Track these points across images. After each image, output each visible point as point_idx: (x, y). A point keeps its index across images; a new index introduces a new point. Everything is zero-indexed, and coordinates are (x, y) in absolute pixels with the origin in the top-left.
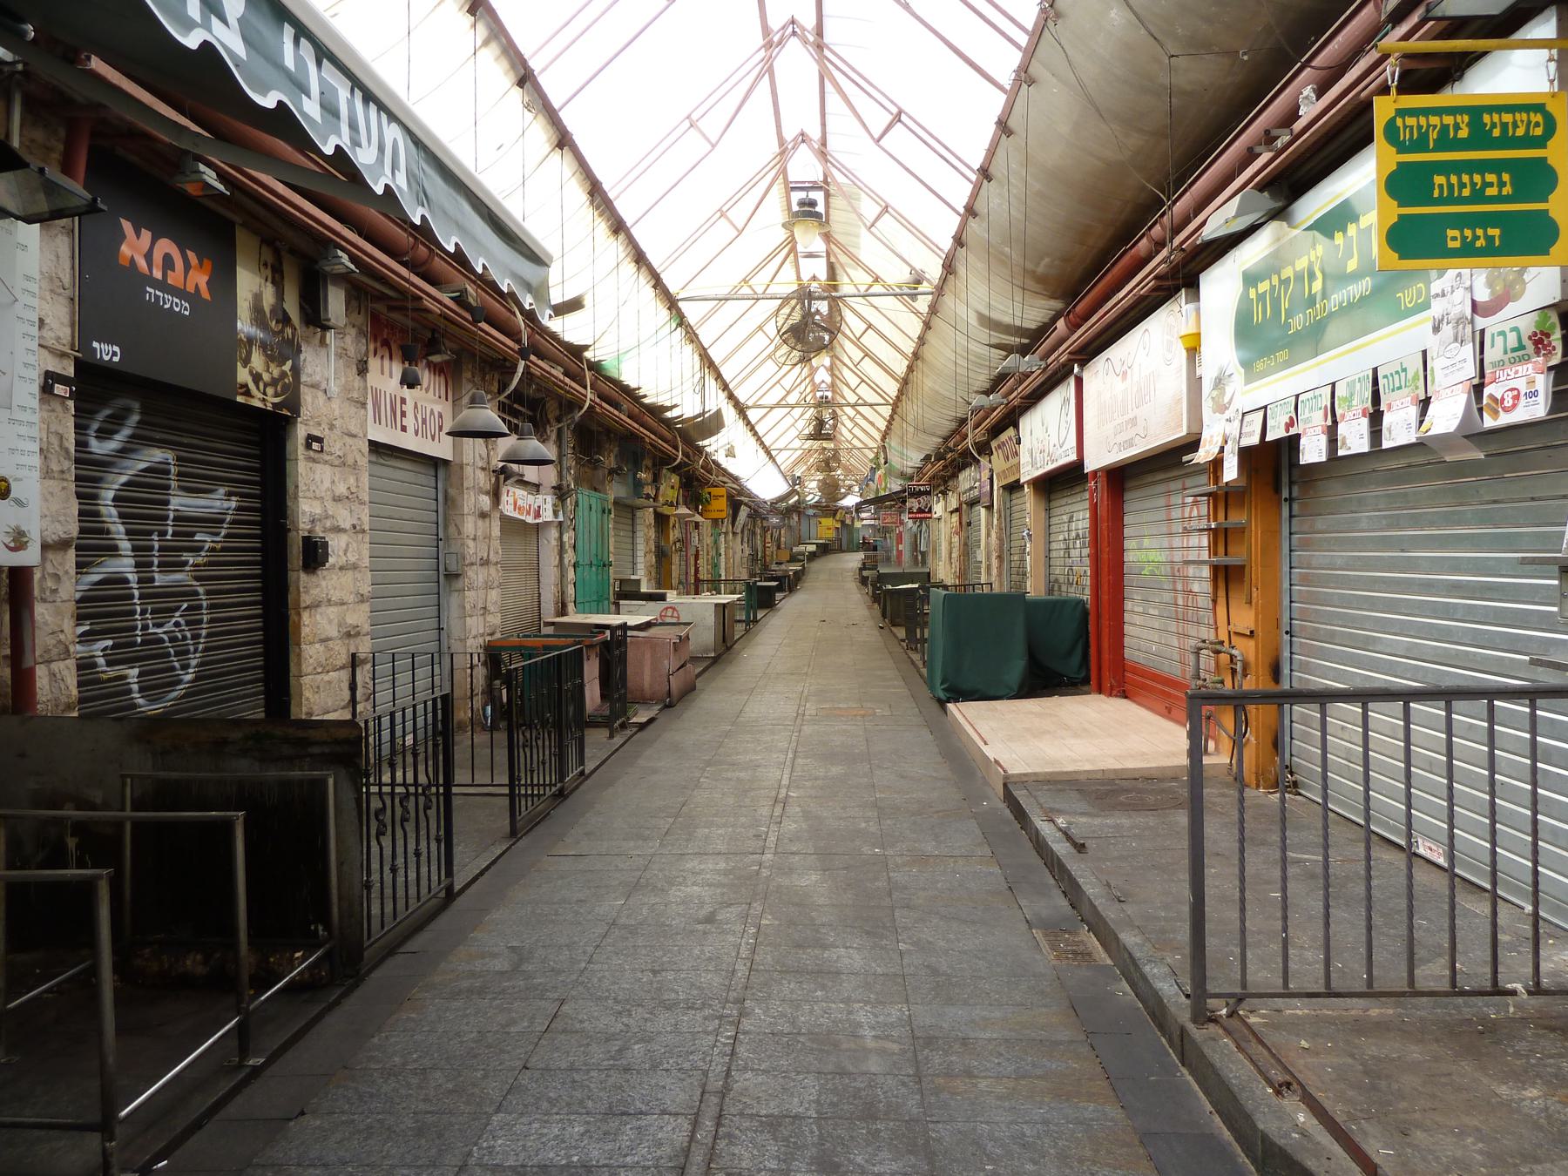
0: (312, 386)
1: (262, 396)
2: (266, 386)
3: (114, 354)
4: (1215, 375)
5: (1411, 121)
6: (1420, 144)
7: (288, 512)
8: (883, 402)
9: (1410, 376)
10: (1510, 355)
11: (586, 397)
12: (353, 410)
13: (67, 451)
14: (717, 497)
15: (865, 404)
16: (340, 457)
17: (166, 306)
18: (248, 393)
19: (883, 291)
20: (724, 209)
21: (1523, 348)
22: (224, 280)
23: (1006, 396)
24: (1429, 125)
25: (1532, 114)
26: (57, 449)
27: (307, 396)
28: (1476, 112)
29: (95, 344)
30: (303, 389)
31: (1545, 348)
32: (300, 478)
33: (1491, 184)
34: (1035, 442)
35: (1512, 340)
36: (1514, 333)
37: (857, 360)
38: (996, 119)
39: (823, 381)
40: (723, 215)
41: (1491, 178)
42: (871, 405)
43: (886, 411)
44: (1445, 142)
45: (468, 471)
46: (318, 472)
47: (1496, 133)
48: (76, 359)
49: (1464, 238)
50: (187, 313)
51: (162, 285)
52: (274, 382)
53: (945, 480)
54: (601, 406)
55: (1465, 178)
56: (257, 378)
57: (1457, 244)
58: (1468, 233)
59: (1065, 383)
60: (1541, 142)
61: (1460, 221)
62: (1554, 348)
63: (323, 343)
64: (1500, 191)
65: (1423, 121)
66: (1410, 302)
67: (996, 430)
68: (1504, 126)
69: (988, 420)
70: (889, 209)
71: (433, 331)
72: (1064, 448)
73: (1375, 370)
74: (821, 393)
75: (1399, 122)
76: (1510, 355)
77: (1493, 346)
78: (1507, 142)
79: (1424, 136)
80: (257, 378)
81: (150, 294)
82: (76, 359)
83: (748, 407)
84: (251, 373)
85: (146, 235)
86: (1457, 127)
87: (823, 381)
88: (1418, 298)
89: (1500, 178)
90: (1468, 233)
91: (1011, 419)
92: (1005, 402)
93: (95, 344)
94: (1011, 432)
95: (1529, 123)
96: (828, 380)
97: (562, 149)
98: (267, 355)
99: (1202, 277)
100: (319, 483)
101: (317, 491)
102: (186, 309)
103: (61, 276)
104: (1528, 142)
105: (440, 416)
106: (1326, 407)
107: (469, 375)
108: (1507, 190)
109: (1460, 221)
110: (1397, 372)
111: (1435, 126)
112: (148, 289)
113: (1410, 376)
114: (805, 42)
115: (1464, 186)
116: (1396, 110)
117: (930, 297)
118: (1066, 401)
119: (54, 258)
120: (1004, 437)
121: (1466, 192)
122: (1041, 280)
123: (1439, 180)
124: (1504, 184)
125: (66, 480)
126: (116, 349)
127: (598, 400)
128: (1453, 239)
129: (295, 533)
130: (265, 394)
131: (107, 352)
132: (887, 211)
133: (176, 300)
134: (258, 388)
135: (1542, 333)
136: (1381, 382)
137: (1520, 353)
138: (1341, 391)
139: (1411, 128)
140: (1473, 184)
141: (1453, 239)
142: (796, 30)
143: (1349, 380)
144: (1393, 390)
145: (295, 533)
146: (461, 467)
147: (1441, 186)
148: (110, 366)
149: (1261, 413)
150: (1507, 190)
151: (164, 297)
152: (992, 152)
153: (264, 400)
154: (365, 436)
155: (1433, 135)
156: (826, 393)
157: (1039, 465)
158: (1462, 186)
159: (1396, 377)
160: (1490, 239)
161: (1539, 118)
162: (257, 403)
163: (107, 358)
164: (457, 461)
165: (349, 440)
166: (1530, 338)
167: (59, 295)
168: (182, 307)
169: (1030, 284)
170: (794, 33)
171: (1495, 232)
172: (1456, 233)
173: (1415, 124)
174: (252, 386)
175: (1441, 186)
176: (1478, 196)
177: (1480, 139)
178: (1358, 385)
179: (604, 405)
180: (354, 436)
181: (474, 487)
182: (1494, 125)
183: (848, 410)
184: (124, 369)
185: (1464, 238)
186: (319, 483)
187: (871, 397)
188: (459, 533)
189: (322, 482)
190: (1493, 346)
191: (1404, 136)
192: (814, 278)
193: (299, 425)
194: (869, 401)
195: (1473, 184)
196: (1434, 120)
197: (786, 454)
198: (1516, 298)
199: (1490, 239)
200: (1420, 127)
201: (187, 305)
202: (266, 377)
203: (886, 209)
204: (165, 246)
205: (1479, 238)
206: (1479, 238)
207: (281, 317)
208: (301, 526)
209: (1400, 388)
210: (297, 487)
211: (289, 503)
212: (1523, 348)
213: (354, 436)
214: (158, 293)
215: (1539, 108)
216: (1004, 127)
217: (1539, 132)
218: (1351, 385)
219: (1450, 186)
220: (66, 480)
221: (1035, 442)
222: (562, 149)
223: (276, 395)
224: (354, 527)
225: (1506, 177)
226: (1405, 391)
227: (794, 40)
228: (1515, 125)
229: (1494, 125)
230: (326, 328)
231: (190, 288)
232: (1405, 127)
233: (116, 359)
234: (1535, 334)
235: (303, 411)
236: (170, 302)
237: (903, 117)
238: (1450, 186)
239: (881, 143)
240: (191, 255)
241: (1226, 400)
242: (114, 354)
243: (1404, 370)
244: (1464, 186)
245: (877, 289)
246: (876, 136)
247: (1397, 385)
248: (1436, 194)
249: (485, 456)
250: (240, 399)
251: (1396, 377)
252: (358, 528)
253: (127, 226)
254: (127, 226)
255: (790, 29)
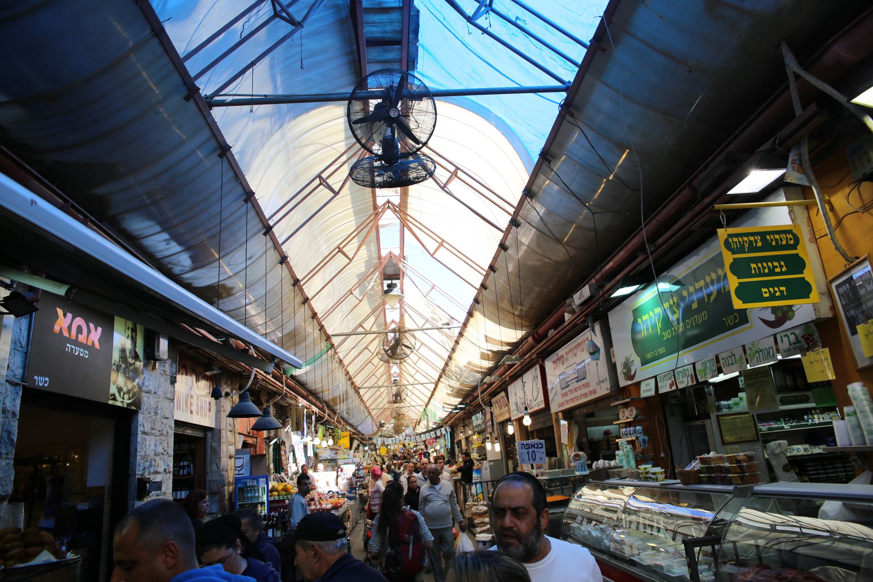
0: (147, 392)
1: (122, 400)
2: (124, 394)
3: (46, 382)
4: (624, 361)
5: (735, 240)
6: (741, 250)
7: (131, 465)
8: (429, 382)
9: (737, 358)
10: (793, 346)
11: (283, 388)
12: (167, 404)
13: (12, 440)
14: (344, 437)
15: (420, 384)
16: (159, 431)
17: (76, 354)
18: (115, 399)
19: (430, 326)
20: (341, 246)
21: (800, 342)
22: (107, 338)
23: (500, 376)
24: (743, 241)
25: (787, 235)
26: (6, 440)
27: (145, 397)
28: (763, 234)
29: (36, 377)
30: (143, 394)
31: (811, 341)
32: (138, 445)
33: (777, 267)
34: (518, 399)
35: (792, 337)
36: (786, 338)
37: (415, 361)
38: (499, 244)
39: (395, 372)
40: (340, 251)
41: (776, 264)
42: (422, 384)
43: (433, 386)
44: (752, 249)
45: (223, 433)
46: (148, 440)
47: (774, 243)
48: (24, 387)
49: (770, 292)
50: (87, 357)
51: (76, 343)
52: (129, 392)
53: (464, 420)
54: (289, 393)
55: (765, 265)
56: (120, 390)
57: (767, 295)
58: (771, 289)
59: (534, 368)
60: (794, 247)
61: (767, 284)
62: (817, 342)
63: (154, 368)
64: (781, 270)
65: (740, 239)
66: (731, 322)
67: (494, 394)
68: (776, 240)
69: (490, 389)
70: (445, 244)
71: (209, 358)
72: (537, 402)
73: (717, 357)
74: (394, 379)
75: (730, 240)
76: (793, 346)
77: (782, 342)
78: (779, 247)
79: (742, 246)
80: (120, 390)
81: (69, 347)
82: (24, 387)
83: (360, 388)
84: (117, 387)
85: (69, 316)
86: (756, 242)
87: (395, 372)
88: (735, 321)
89: (780, 264)
90: (771, 289)
91: (503, 388)
92: (500, 379)
93: (36, 377)
94: (503, 394)
95: (787, 238)
96: (398, 371)
97: (282, 264)
98: (126, 377)
99: (610, 314)
100: (148, 447)
101: (147, 452)
102: (86, 355)
103: (21, 340)
104: (788, 247)
105: (210, 404)
106: (692, 375)
107: (225, 380)
108: (784, 269)
109: (767, 284)
110: (730, 356)
111: (746, 242)
112: (68, 345)
113: (737, 358)
114: (395, 211)
115: (765, 268)
116: (728, 235)
117: (564, 95)
118: (535, 377)
119: (19, 331)
120: (498, 397)
121: (766, 271)
122: (520, 317)
123: (753, 266)
124: (782, 266)
125: (9, 458)
126: (47, 379)
127: (288, 390)
128: (766, 293)
129: (133, 477)
130: (123, 398)
131: (42, 381)
132: (442, 245)
133: (82, 350)
134: (120, 395)
135: (808, 334)
136: (722, 361)
137: (799, 345)
138: (699, 366)
139: (736, 242)
140: (769, 267)
141: (766, 293)
142: (390, 205)
143: (703, 361)
144: (729, 365)
145: (133, 477)
146: (220, 431)
147: (754, 268)
148: (43, 389)
149: (653, 380)
150: (784, 269)
151: (75, 349)
152: (495, 258)
153: (123, 402)
154: (173, 418)
155: (746, 245)
156: (397, 378)
157: (522, 411)
158: (764, 268)
159: (730, 359)
160: (781, 292)
161: (790, 236)
162: (119, 404)
163: (41, 385)
164: (218, 428)
165: (164, 421)
166: (802, 337)
167: (19, 351)
168: (84, 354)
169: (518, 320)
170: (389, 207)
171: (783, 289)
172: (766, 290)
173: (753, 240)
174: (117, 395)
175: (754, 268)
176: (772, 272)
177: (767, 246)
178: (708, 364)
179: (292, 392)
180: (167, 418)
181: (226, 442)
182: (772, 240)
183: (410, 387)
184: (52, 391)
185: (770, 292)
186: (148, 447)
187: (422, 380)
188: (218, 468)
189: (150, 446)
190: (782, 342)
191: (733, 246)
192: (393, 321)
193: (140, 415)
194: (422, 382)
195: (769, 267)
196: (745, 239)
197: (375, 411)
198: (790, 318)
199: (781, 292)
200: (740, 242)
201: (87, 352)
202: (125, 389)
203: (441, 245)
204: (79, 321)
205: (776, 292)
206: (776, 292)
207: (133, 356)
208: (138, 472)
209: (732, 364)
210: (136, 450)
211: (131, 460)
212: (800, 342)
213: (167, 418)
214: (73, 347)
215: (789, 232)
216: (503, 246)
217: (792, 242)
218: (704, 364)
219: (759, 268)
220: (9, 458)
221: (518, 399)
222: (282, 264)
223: (129, 399)
224: (165, 470)
225: (782, 263)
226: (735, 366)
227: (389, 210)
228: (781, 240)
229: (772, 240)
230: (156, 360)
231: (90, 344)
232: (733, 242)
233: (46, 385)
234: (805, 335)
235: (142, 406)
236: (78, 351)
237: (460, 174)
238: (759, 268)
239: (435, 256)
240: (92, 326)
241: (632, 373)
242: (46, 382)
243: (734, 355)
244: (765, 268)
245: (428, 326)
246: (432, 253)
247: (731, 362)
248: (753, 272)
249: (232, 424)
250: (110, 402)
251: (730, 359)
252: (167, 471)
253: (60, 312)
254: (60, 312)
255: (387, 205)
